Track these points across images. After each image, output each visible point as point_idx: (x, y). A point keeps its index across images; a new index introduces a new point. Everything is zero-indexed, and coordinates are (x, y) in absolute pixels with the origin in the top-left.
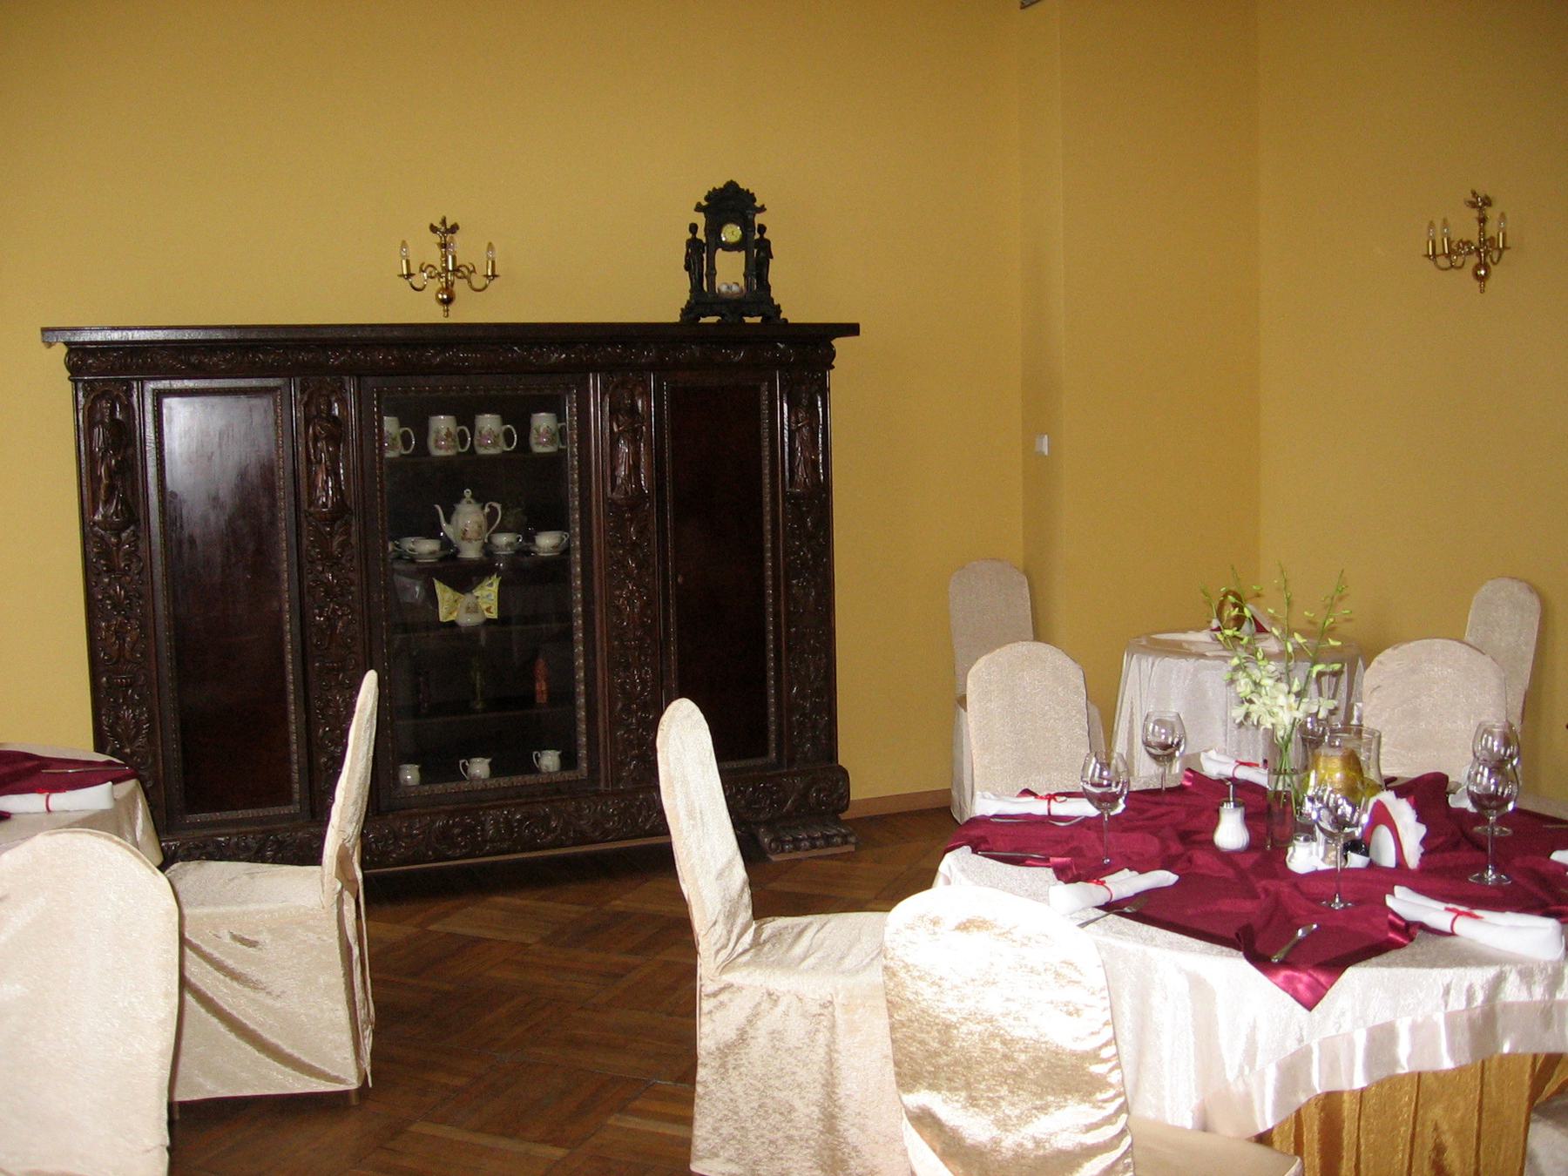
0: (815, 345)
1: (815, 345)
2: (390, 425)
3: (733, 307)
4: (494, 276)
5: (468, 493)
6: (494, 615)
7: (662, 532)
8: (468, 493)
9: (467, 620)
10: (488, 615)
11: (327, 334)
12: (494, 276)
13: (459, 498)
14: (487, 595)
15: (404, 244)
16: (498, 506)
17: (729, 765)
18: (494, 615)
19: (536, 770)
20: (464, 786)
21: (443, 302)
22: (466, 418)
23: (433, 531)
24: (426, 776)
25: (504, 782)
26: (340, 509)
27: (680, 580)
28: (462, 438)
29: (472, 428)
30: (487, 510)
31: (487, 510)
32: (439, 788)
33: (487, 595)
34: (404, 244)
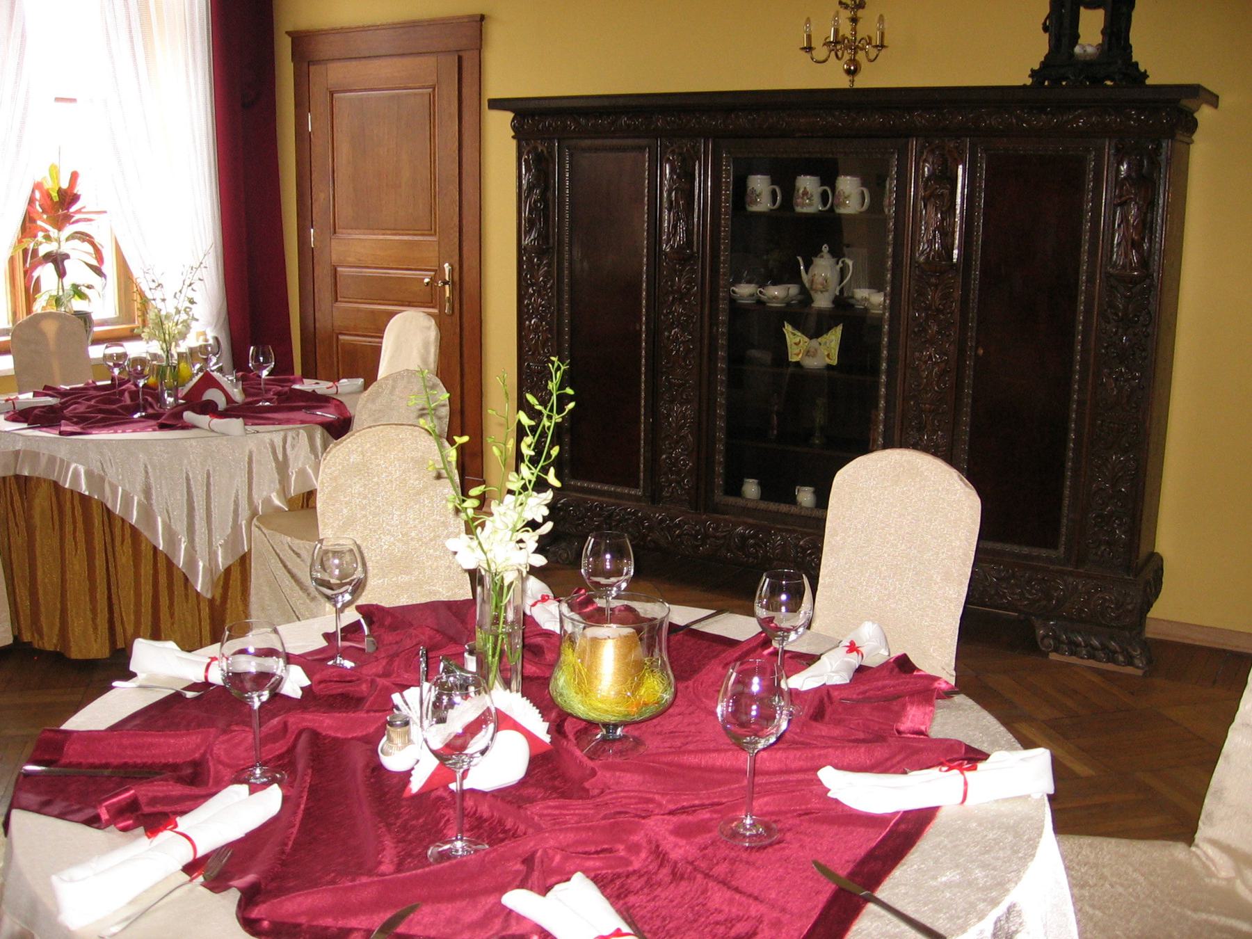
0: (1175, 111)
1: (1175, 111)
2: (760, 184)
3: (1091, 70)
4: (882, 46)
5: (825, 248)
6: (834, 362)
7: (965, 301)
8: (825, 248)
9: (813, 363)
10: (828, 361)
11: (532, 105)
12: (882, 46)
13: (817, 252)
14: (833, 339)
15: (808, 20)
16: (850, 263)
17: (989, 545)
18: (834, 362)
19: (793, 500)
20: (793, 509)
21: (848, 72)
22: (829, 180)
23: (795, 278)
24: (766, 495)
25: (763, 505)
26: (683, 256)
27: (981, 352)
28: (824, 198)
29: (833, 189)
30: (840, 264)
31: (840, 264)
32: (773, 506)
33: (833, 339)
34: (808, 20)
